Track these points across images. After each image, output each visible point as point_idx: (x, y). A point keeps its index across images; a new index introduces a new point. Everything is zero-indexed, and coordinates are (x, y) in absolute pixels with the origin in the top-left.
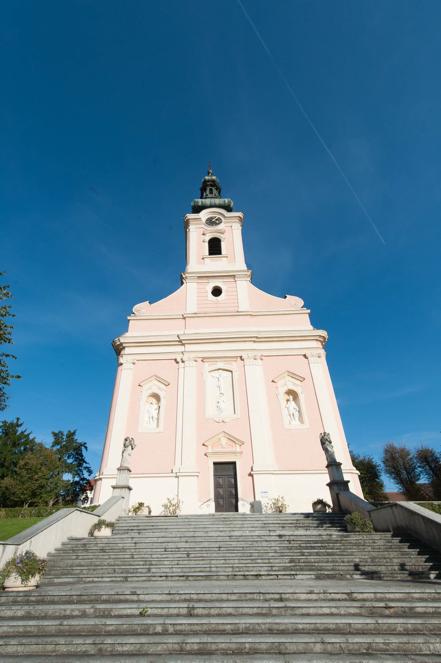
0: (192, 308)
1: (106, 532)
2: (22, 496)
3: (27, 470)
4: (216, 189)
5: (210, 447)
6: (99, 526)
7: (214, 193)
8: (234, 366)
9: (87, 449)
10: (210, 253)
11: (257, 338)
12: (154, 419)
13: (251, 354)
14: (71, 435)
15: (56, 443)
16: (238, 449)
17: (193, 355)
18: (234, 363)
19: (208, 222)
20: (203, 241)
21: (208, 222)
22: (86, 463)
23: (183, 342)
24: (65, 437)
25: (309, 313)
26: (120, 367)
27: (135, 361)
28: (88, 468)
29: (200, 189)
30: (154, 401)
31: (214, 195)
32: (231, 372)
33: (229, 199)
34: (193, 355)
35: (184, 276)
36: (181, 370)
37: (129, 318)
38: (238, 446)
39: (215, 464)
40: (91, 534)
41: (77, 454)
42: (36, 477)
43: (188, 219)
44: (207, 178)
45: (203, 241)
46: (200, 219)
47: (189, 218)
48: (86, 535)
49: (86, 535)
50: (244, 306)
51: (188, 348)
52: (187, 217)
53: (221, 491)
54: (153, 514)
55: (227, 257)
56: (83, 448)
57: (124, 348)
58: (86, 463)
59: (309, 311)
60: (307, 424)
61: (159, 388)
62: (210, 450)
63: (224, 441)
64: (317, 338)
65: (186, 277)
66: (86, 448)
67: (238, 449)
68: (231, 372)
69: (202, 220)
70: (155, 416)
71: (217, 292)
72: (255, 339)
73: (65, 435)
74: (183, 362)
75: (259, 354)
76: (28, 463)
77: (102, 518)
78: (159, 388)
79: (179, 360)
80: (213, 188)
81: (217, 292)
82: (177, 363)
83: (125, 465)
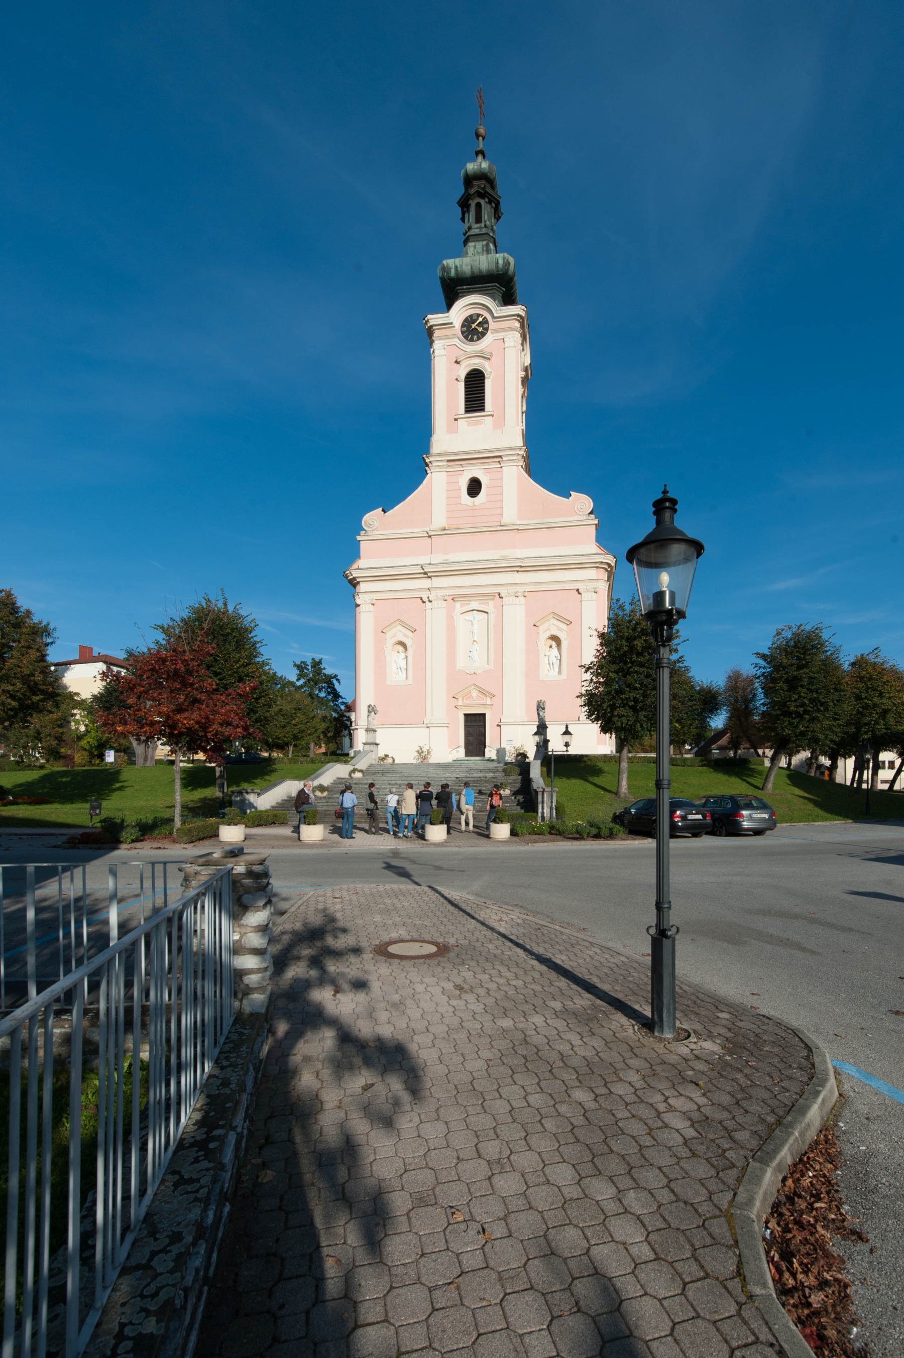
0: (439, 519)
1: (358, 775)
2: (285, 739)
3: (283, 715)
4: (490, 202)
5: (460, 700)
6: (354, 771)
7: (483, 220)
8: (490, 606)
9: (339, 683)
10: (468, 410)
11: (521, 567)
12: (403, 669)
13: (512, 590)
14: (317, 664)
15: (300, 676)
16: (489, 701)
17: (441, 593)
18: (491, 603)
19: (465, 329)
20: (457, 379)
21: (465, 329)
22: (342, 698)
23: (429, 574)
24: (309, 667)
25: (596, 525)
26: (358, 608)
27: (374, 601)
28: (345, 703)
29: (458, 203)
30: (401, 648)
31: (483, 225)
32: (487, 613)
33: (506, 255)
34: (441, 593)
35: (427, 460)
36: (428, 612)
37: (358, 538)
38: (489, 699)
39: (465, 715)
40: (350, 775)
41: (329, 687)
42: (294, 722)
43: (431, 326)
44: (471, 167)
45: (457, 379)
46: (451, 323)
47: (431, 323)
48: (347, 776)
49: (347, 776)
50: (510, 515)
51: (437, 582)
52: (428, 320)
53: (471, 738)
54: (396, 762)
55: (492, 415)
56: (334, 681)
57: (358, 583)
58: (342, 698)
59: (596, 522)
60: (564, 675)
61: (405, 636)
62: (460, 703)
63: (475, 693)
64: (598, 565)
65: (430, 462)
66: (338, 680)
67: (489, 701)
68: (487, 613)
69: (454, 327)
70: (403, 665)
71: (474, 487)
72: (518, 569)
73: (310, 665)
74: (430, 601)
75: (521, 589)
76: (281, 709)
77: (356, 767)
78: (405, 636)
79: (425, 599)
80: (482, 202)
81: (474, 487)
82: (424, 602)
83: (371, 727)
